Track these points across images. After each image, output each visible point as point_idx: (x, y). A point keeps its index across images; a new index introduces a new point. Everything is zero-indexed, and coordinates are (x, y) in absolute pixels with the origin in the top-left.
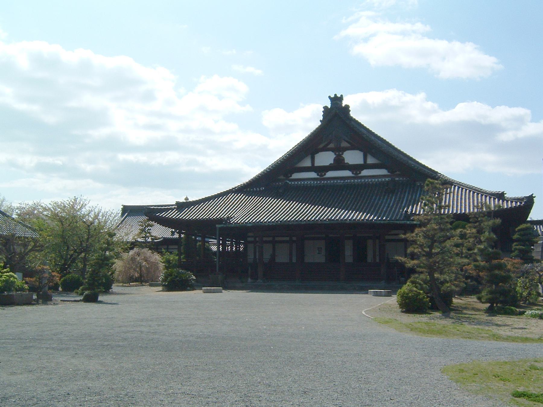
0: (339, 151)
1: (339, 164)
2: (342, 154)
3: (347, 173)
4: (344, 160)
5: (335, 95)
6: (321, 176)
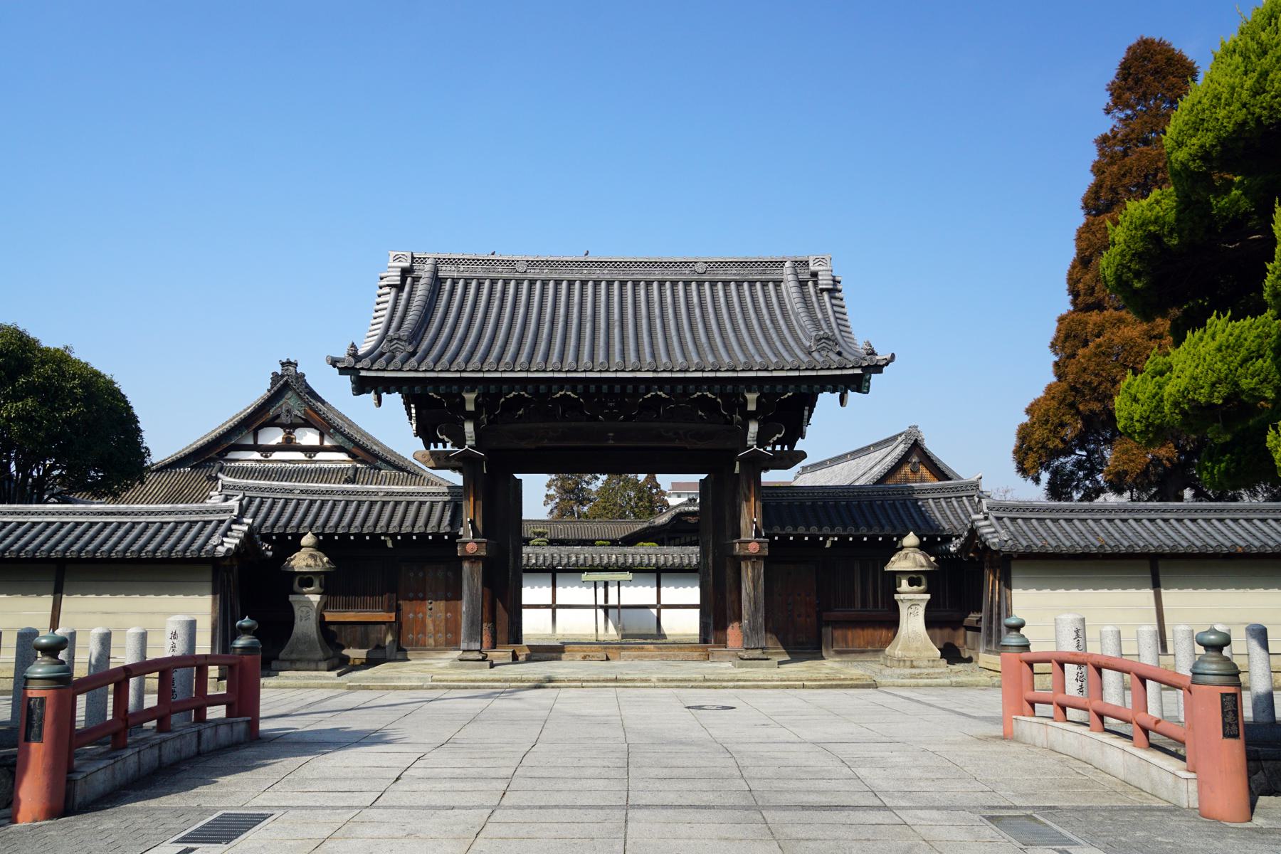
1: (289, 445)
3: (299, 456)
6: (310, 457)
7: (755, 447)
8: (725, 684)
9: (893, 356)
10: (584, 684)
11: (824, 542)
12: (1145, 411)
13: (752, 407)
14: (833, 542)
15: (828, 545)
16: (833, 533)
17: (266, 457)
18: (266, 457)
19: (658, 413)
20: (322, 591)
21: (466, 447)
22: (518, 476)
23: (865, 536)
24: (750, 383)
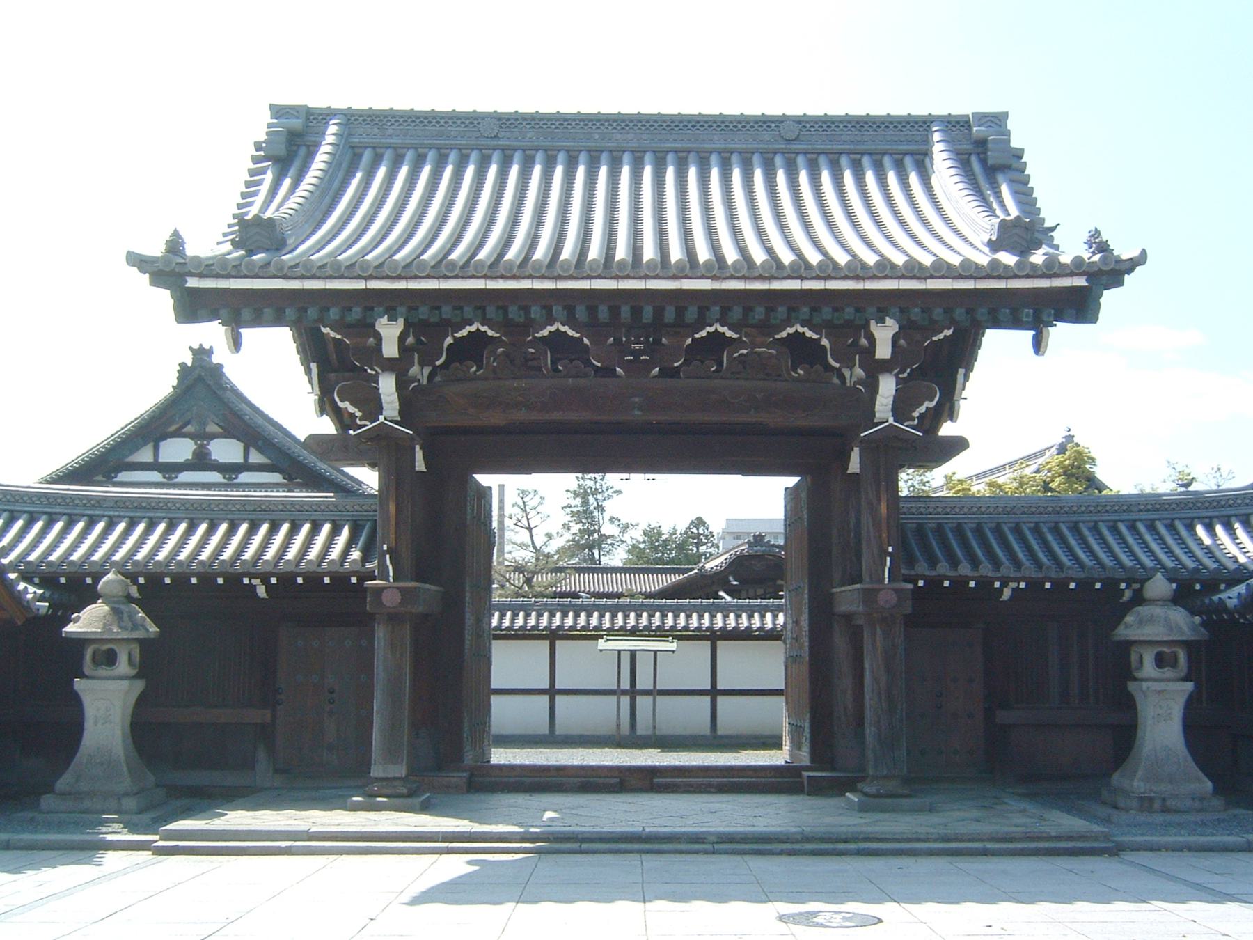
0: (202, 437)
1: (201, 461)
2: (208, 444)
3: (216, 477)
4: (209, 454)
5: (201, 345)
6: (230, 479)
7: (891, 420)
8: (841, 846)
9: (1144, 253)
10: (584, 846)
11: (1000, 591)
12: (1048, 477)
13: (883, 351)
14: (1016, 591)
15: (1007, 594)
16: (1019, 575)
17: (170, 479)
18: (170, 479)
19: (720, 364)
20: (133, 672)
21: (381, 418)
22: (484, 479)
23: (1073, 580)
24: (883, 303)
